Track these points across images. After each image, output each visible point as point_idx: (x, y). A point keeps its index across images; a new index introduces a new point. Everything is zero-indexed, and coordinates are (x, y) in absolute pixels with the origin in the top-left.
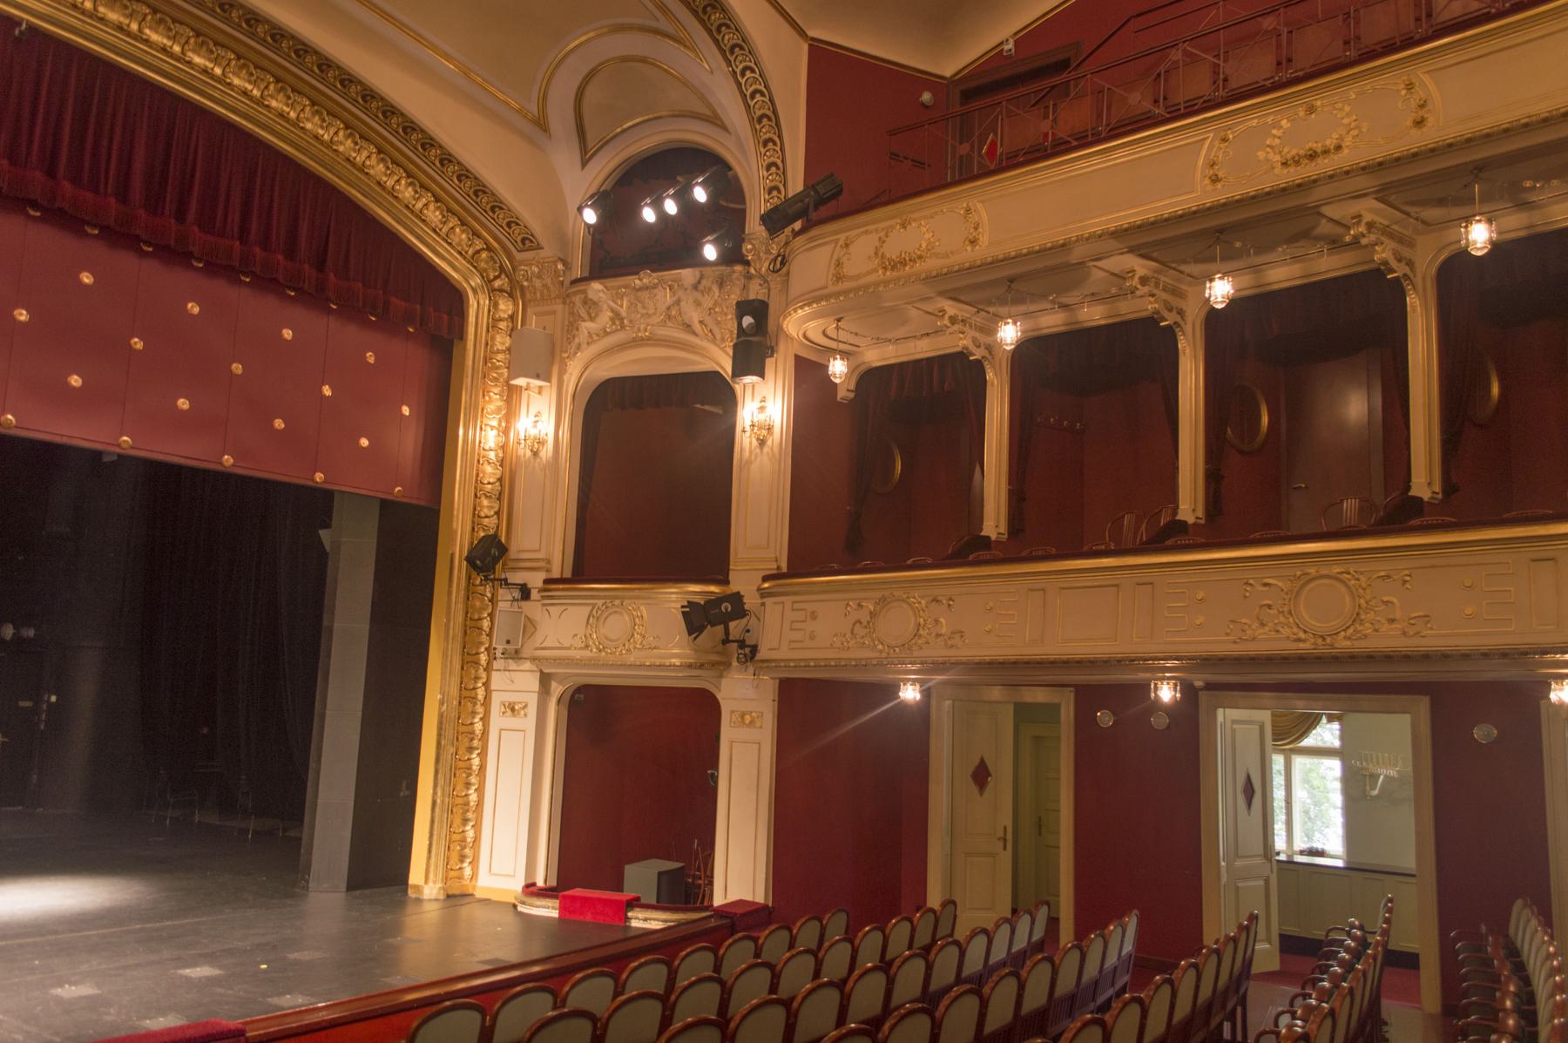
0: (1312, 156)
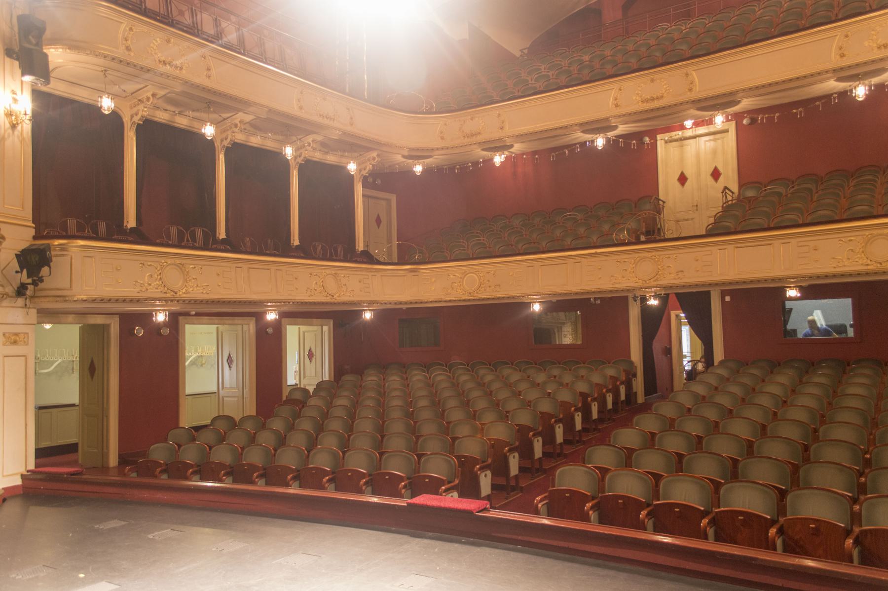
0: (653, 99)
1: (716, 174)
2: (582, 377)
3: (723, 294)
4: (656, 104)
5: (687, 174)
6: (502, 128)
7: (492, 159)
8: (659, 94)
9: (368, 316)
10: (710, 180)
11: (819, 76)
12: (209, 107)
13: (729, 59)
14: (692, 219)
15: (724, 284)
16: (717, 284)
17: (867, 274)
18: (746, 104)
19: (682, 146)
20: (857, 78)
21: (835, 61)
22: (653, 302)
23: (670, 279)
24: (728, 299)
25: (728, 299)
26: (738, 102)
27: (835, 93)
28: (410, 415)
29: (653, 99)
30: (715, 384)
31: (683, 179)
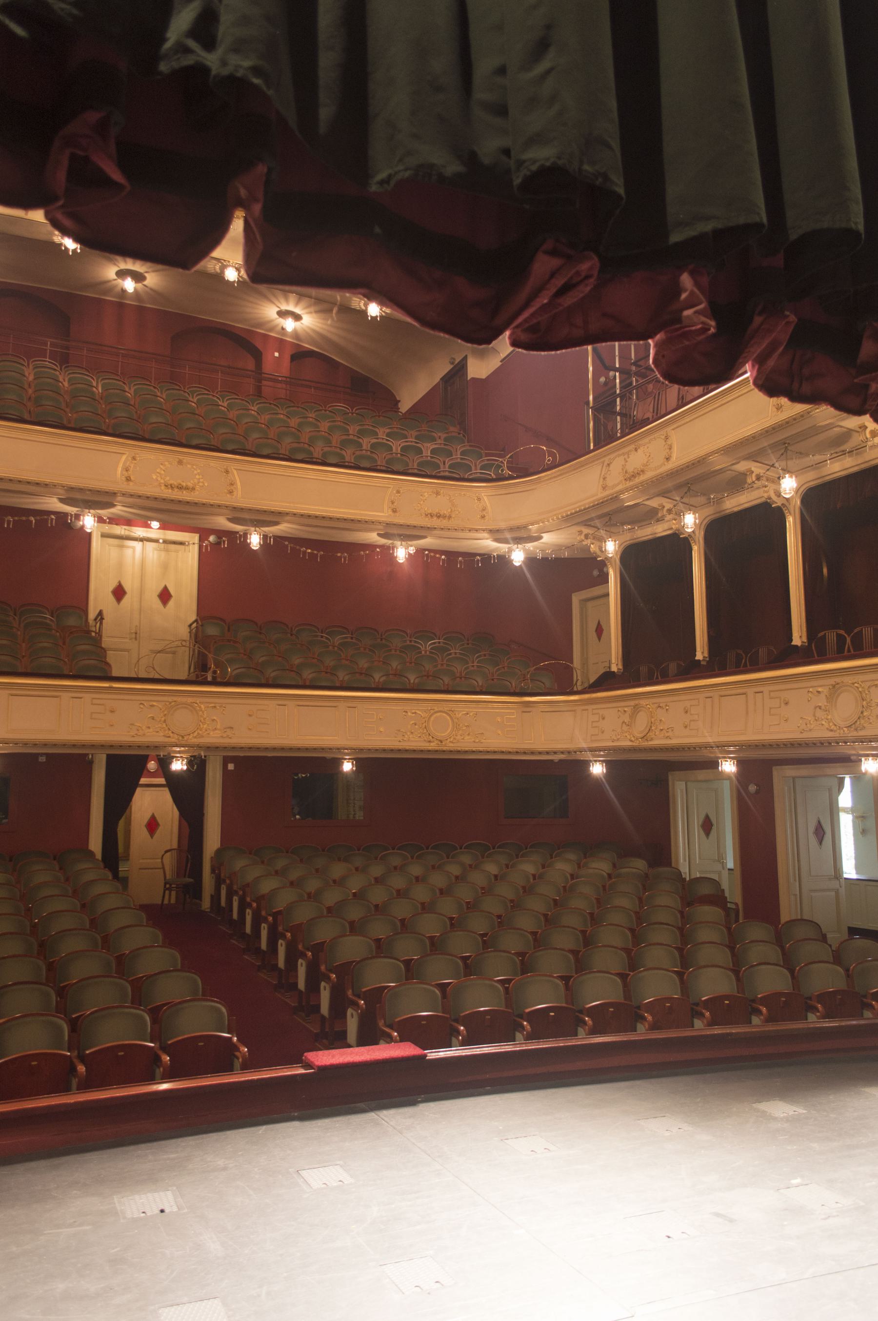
1: (165, 596)
2: (395, 868)
3: (226, 760)
4: (185, 496)
5: (127, 587)
6: (231, 492)
7: (246, 535)
8: (190, 485)
9: (347, 766)
10: (157, 603)
11: (46, 487)
12: (786, 449)
13: (43, 438)
14: (128, 651)
15: (111, 746)
16: (102, 746)
17: (112, 746)
18: (284, 528)
19: (122, 547)
20: (258, 523)
21: (384, 515)
22: (178, 766)
23: (214, 735)
24: (231, 767)
25: (231, 767)
26: (113, 506)
27: (480, 555)
28: (548, 920)
29: (180, 488)
30: (533, 872)
31: (119, 593)
